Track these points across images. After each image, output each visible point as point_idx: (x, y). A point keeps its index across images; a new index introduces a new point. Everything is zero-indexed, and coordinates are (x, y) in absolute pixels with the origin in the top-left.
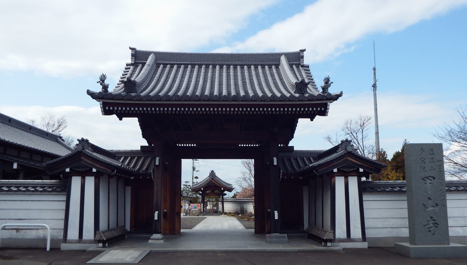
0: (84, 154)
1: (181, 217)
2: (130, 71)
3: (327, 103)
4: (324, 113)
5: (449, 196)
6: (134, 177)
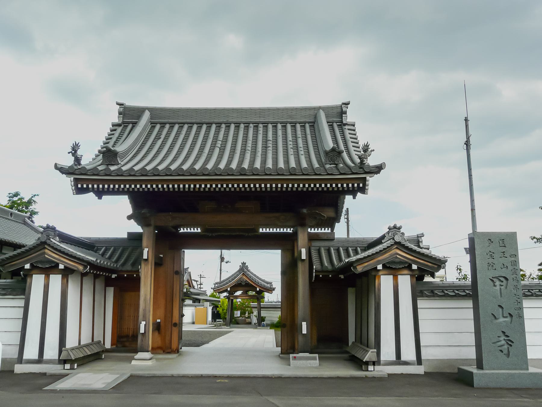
0: (49, 245)
1: (184, 329)
2: (117, 134)
3: (365, 178)
4: (363, 190)
5: (527, 303)
6: (116, 275)
